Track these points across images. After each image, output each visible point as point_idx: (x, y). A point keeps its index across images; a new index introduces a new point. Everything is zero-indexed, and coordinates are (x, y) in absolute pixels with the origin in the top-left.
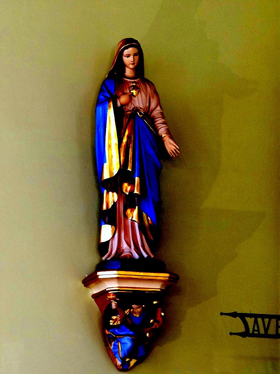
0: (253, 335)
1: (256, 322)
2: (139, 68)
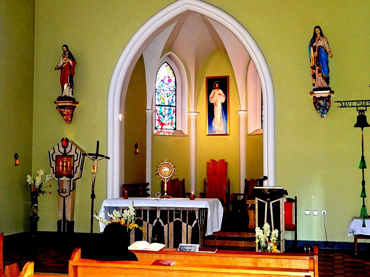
0: (344, 107)
1: (345, 103)
2: (322, 34)
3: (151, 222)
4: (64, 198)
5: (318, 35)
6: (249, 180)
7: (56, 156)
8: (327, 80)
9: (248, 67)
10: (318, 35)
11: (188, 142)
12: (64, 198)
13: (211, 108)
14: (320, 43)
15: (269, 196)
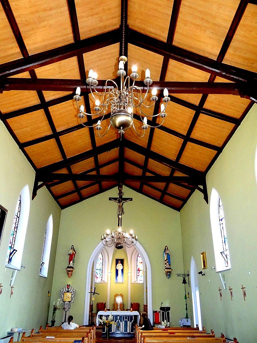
3: (116, 321)
4: (66, 311)
5: (166, 249)
6: (132, 303)
7: (64, 292)
8: (170, 265)
9: (132, 255)
10: (166, 249)
11: (107, 286)
12: (66, 311)
13: (117, 271)
14: (167, 252)
15: (166, 310)
